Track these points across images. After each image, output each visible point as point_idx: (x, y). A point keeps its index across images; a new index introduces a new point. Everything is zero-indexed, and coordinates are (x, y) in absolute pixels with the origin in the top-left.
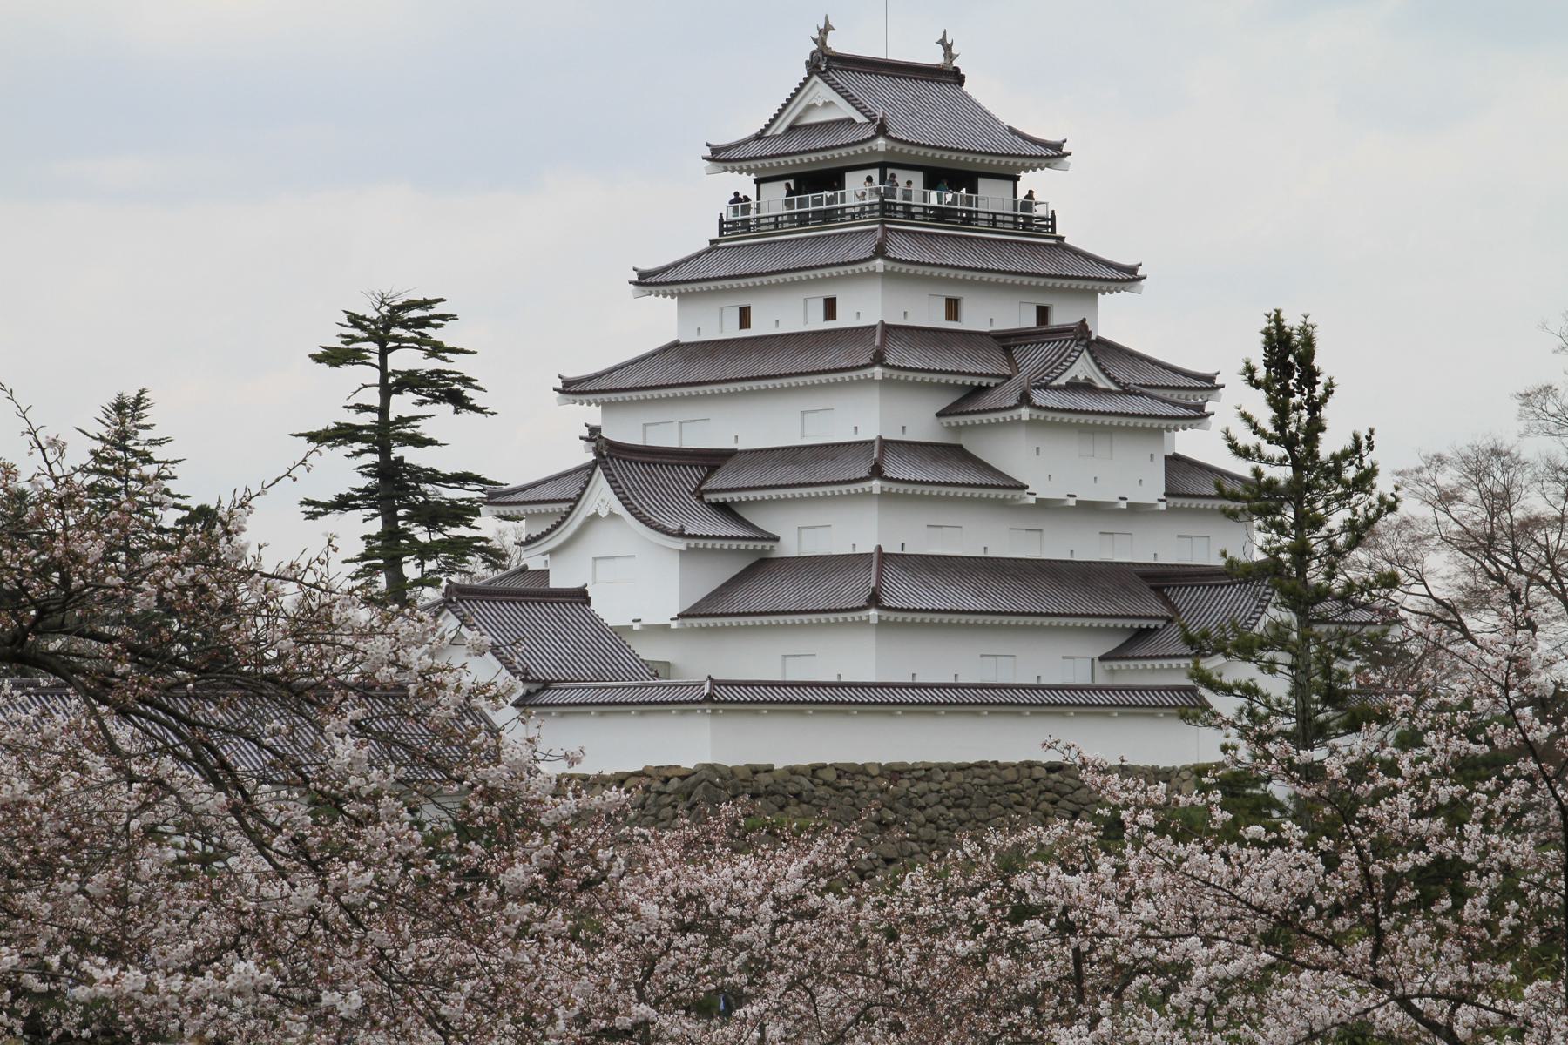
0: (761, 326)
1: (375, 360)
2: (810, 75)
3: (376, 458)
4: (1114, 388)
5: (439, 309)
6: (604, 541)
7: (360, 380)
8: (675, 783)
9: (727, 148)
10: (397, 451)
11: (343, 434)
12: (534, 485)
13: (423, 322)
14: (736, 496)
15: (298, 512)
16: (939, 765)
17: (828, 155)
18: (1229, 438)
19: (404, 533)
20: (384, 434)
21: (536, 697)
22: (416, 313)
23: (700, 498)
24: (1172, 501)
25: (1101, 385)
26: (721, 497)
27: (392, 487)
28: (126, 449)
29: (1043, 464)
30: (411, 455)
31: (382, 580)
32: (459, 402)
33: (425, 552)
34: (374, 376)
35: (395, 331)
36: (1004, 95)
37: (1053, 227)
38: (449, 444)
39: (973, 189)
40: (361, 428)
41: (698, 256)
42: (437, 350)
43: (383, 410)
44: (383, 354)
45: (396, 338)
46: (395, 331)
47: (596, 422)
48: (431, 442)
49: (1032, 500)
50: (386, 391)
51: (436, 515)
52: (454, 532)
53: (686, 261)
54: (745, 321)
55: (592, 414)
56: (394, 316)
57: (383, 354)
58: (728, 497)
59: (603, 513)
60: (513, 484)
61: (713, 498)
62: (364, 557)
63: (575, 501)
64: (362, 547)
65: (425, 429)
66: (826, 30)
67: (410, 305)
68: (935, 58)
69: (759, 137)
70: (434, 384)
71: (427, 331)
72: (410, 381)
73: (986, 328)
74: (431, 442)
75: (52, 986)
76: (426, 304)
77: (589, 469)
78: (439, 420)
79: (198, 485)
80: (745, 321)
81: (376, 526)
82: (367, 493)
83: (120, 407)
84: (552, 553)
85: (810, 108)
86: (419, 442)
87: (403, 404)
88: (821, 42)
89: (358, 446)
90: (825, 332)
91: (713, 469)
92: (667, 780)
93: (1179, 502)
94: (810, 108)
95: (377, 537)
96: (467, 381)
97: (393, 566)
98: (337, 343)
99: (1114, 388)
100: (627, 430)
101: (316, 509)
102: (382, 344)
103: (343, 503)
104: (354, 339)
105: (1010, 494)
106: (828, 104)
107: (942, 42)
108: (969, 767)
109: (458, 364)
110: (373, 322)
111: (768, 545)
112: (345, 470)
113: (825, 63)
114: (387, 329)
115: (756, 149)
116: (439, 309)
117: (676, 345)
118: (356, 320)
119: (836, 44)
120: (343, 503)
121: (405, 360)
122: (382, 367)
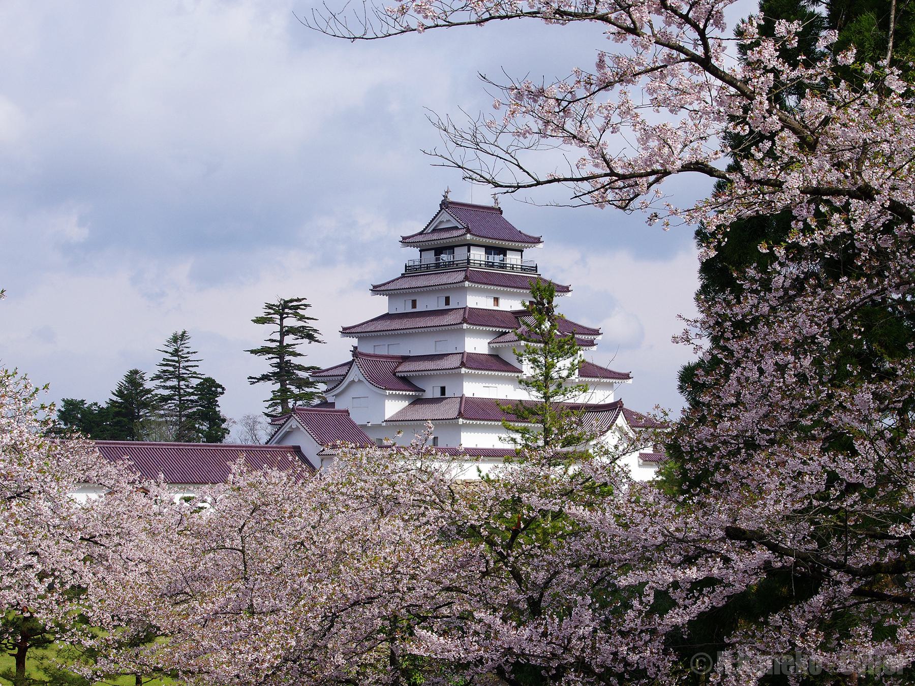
0: (420, 308)
1: (278, 321)
2: (442, 209)
3: (278, 360)
5: (303, 302)
6: (356, 391)
9: (409, 237)
10: (287, 358)
11: (264, 351)
12: (332, 369)
13: (297, 307)
14: (408, 374)
15: (247, 382)
17: (448, 241)
18: (252, 352)
19: (289, 390)
20: (281, 351)
22: (295, 303)
23: (394, 374)
26: (402, 374)
27: (284, 372)
28: (178, 356)
30: (295, 360)
31: (280, 409)
32: (311, 338)
33: (297, 398)
34: (278, 328)
35: (286, 310)
38: (309, 355)
39: (505, 255)
40: (272, 348)
41: (397, 279)
42: (302, 318)
43: (281, 342)
44: (282, 319)
45: (287, 314)
46: (286, 310)
47: (356, 345)
48: (300, 355)
50: (283, 334)
51: (302, 383)
52: (307, 390)
53: (393, 281)
54: (414, 306)
55: (354, 341)
56: (285, 304)
57: (282, 319)
58: (405, 374)
60: (323, 368)
61: (399, 374)
62: (272, 399)
63: (345, 376)
64: (272, 396)
65: (297, 349)
67: (292, 301)
69: (421, 233)
70: (300, 332)
71: (299, 311)
72: (292, 330)
73: (509, 310)
74: (300, 355)
75: (679, 573)
76: (298, 300)
77: (350, 364)
78: (303, 346)
79: (206, 370)
80: (414, 306)
81: (278, 386)
82: (274, 374)
83: (175, 339)
84: (336, 396)
85: (441, 222)
86: (296, 355)
87: (289, 339)
88: (445, 197)
89: (271, 356)
91: (400, 363)
94: (441, 222)
95: (278, 391)
96: (315, 331)
97: (284, 402)
98: (263, 315)
100: (367, 348)
101: (254, 380)
102: (281, 315)
103: (265, 378)
104: (269, 314)
106: (448, 221)
109: (310, 323)
110: (278, 306)
111: (421, 393)
112: (266, 365)
113: (446, 205)
114: (283, 310)
115: (420, 238)
116: (303, 302)
117: (387, 314)
118: (270, 306)
119: (452, 198)
120: (265, 378)
121: (290, 322)
122: (281, 325)
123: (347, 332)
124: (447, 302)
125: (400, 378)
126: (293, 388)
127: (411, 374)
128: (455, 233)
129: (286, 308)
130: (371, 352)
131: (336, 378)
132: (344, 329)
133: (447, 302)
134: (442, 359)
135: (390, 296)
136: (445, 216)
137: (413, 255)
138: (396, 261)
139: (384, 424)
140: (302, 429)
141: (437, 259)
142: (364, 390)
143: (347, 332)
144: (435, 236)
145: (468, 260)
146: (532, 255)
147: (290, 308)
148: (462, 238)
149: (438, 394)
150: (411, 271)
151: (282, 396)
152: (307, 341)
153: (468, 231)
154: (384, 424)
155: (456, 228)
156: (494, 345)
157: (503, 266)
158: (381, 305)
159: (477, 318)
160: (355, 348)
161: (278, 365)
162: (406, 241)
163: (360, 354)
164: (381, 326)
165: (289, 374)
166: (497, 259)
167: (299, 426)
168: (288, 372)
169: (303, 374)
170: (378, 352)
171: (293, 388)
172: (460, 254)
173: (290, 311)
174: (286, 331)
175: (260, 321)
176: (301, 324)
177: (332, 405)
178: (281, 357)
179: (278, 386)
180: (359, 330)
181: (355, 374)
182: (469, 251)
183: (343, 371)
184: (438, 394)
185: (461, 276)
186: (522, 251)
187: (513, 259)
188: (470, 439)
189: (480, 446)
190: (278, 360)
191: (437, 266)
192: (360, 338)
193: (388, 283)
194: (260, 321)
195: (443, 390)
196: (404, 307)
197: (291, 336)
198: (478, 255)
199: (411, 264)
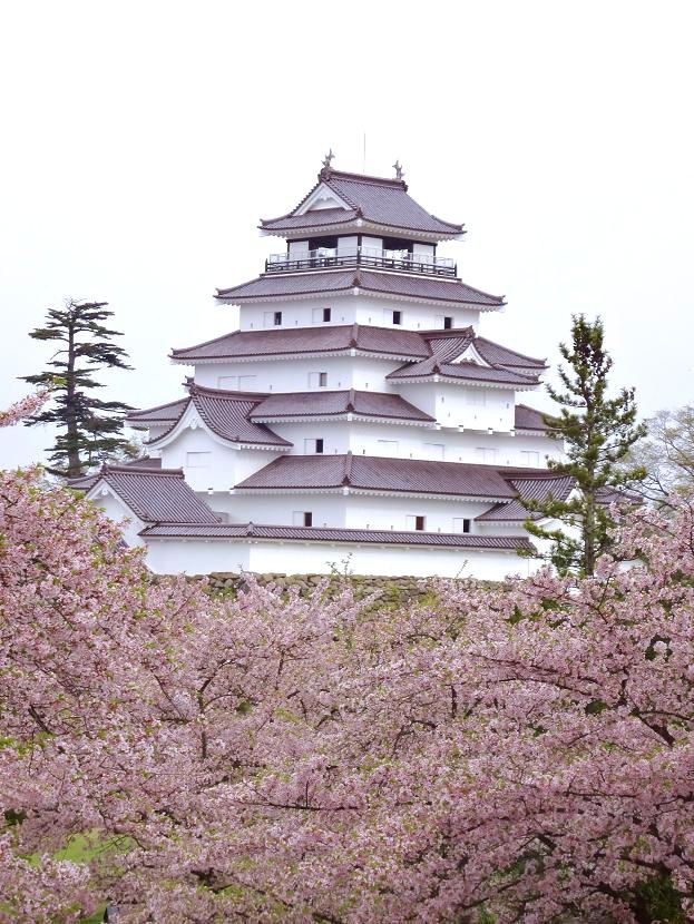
0: (286, 324)
1: (67, 336)
2: (320, 182)
3: (66, 393)
4: (487, 366)
6: (192, 444)
7: (56, 349)
8: (230, 582)
9: (272, 222)
10: (78, 389)
13: (95, 316)
16: (380, 577)
19: (80, 436)
21: (154, 529)
22: (91, 311)
23: (249, 420)
24: (518, 431)
25: (479, 364)
26: (260, 421)
27: (74, 409)
29: (450, 409)
30: (89, 393)
31: (66, 461)
32: (112, 361)
33: (91, 446)
34: (66, 346)
36: (431, 196)
37: (455, 273)
38: (108, 385)
39: (411, 250)
41: (253, 282)
42: (102, 332)
43: (70, 366)
44: (71, 334)
46: (78, 320)
47: (191, 375)
48: (97, 385)
49: (438, 428)
50: (73, 355)
51: (97, 426)
55: (188, 370)
56: (77, 312)
57: (71, 334)
59: (194, 428)
60: (144, 408)
65: (93, 377)
66: (329, 158)
67: (87, 306)
68: (391, 175)
69: (289, 217)
70: (99, 352)
71: (95, 321)
72: (87, 350)
73: (416, 329)
74: (97, 385)
76: (96, 306)
77: (186, 402)
78: (102, 372)
81: (64, 430)
82: (60, 412)
84: (164, 449)
86: (90, 384)
87: (81, 362)
88: (327, 164)
90: (393, 330)
91: (257, 404)
92: (224, 581)
93: (522, 432)
96: (119, 350)
97: (73, 452)
99: (487, 366)
100: (209, 381)
102: (71, 328)
104: (54, 325)
105: (421, 423)
106: (330, 199)
107: (396, 166)
108: (398, 579)
109: (114, 340)
111: (286, 448)
113: (327, 176)
114: (74, 319)
115: (288, 223)
116: (103, 309)
118: (55, 314)
119: (336, 166)
120: (47, 417)
121: (85, 337)
122: (71, 341)
123: (179, 356)
124: (327, 316)
125: (249, 419)
126: (85, 433)
127: (274, 420)
128: (341, 217)
129: (77, 317)
130: (214, 387)
131: (164, 421)
132: (176, 352)
133: (327, 316)
134: (317, 399)
135: (243, 306)
136: (326, 192)
137: (277, 247)
138: (256, 254)
139: (232, 492)
140: (116, 497)
141: (313, 255)
142: (207, 442)
143: (179, 356)
144: (310, 222)
145: (359, 256)
146: (447, 252)
147: (83, 317)
148: (350, 224)
149: (312, 451)
150: (273, 270)
151: (70, 445)
152: (107, 364)
153: (360, 215)
154: (232, 492)
155: (341, 210)
156: (395, 381)
157: (407, 267)
158: (231, 319)
159: (361, 340)
160: (190, 380)
161: (67, 400)
162: (268, 227)
163: (201, 389)
164: (238, 348)
165: (80, 411)
166: (397, 255)
167: (113, 492)
168: (81, 409)
169: (99, 413)
170: (223, 388)
171: (85, 433)
172: (347, 247)
173: (84, 322)
174: (78, 350)
175: (41, 335)
176: (99, 340)
177: (158, 461)
178: (70, 388)
179: (555, 543)
180: (197, 354)
181: (192, 418)
182: (359, 244)
183: (175, 413)
184: (312, 451)
185: (349, 280)
186: (435, 245)
187: (421, 255)
188: (358, 517)
189: (396, 529)
190: (66, 393)
191: (313, 264)
192: (197, 366)
193: (240, 287)
194: (41, 335)
195: (320, 444)
196: (264, 323)
197: (85, 358)
198: (372, 249)
199: (274, 260)
